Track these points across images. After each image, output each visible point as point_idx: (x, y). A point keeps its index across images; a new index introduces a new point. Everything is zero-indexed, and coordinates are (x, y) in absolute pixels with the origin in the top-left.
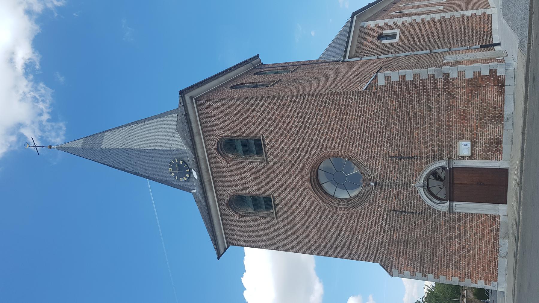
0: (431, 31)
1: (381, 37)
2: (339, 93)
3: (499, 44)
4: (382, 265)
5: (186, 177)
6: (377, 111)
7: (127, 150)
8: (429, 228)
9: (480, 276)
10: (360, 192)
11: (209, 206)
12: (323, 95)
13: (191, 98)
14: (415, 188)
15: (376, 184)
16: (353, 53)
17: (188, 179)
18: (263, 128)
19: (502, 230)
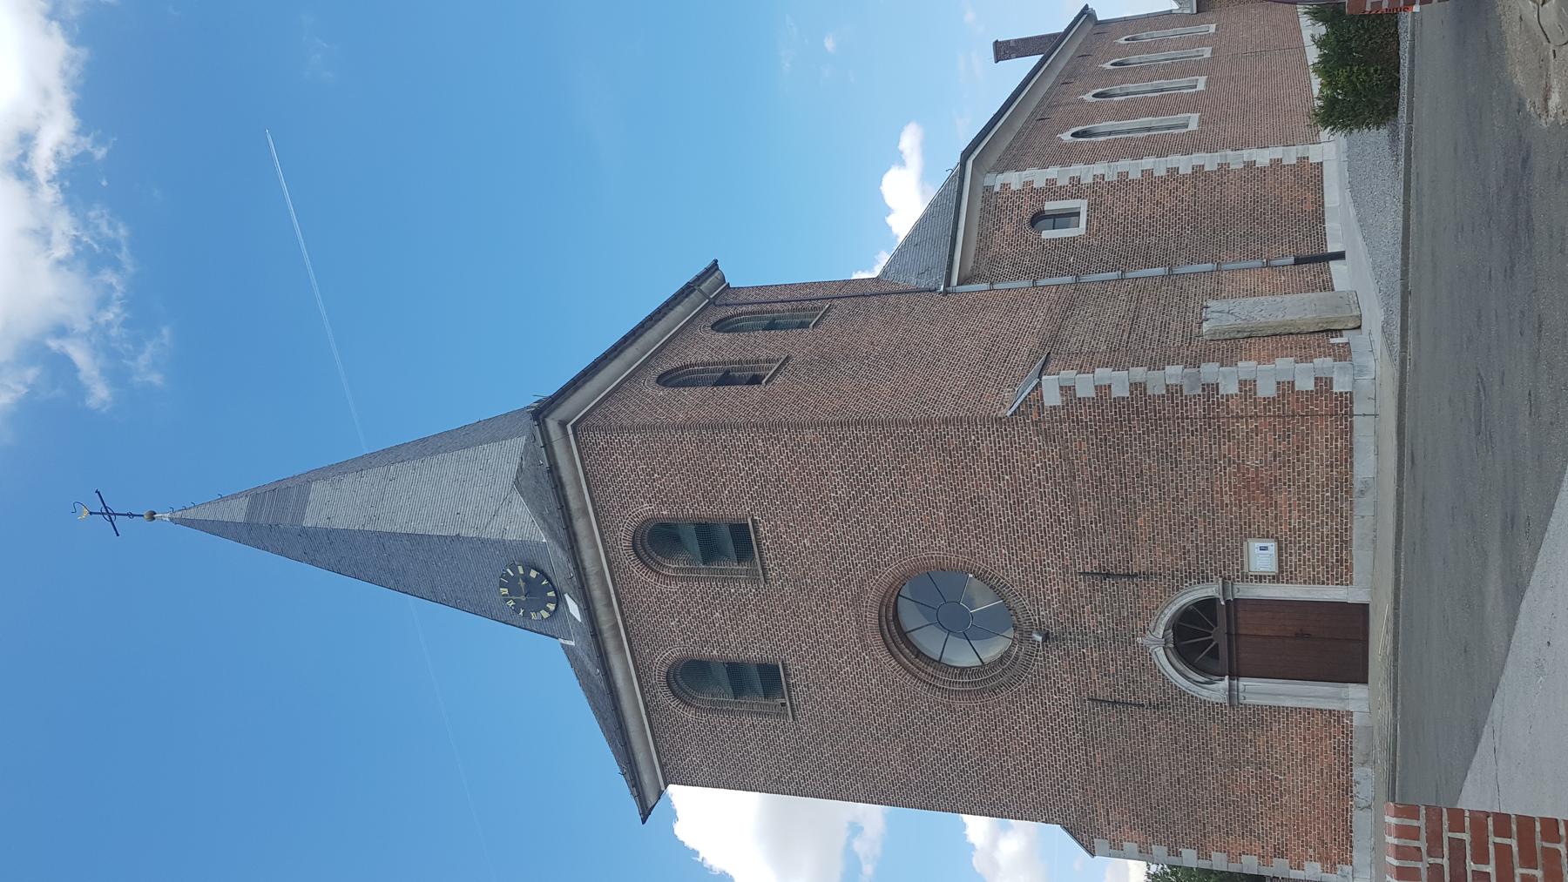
1: (1038, 218)
2: (946, 422)
3: (1340, 256)
4: (1067, 829)
5: (547, 610)
6: (1045, 466)
7: (380, 535)
8: (1182, 741)
9: (1311, 851)
10: (1007, 654)
12: (905, 423)
14: (1145, 648)
15: (1046, 637)
16: (970, 264)
17: (553, 614)
18: (753, 498)
19: (1359, 746)
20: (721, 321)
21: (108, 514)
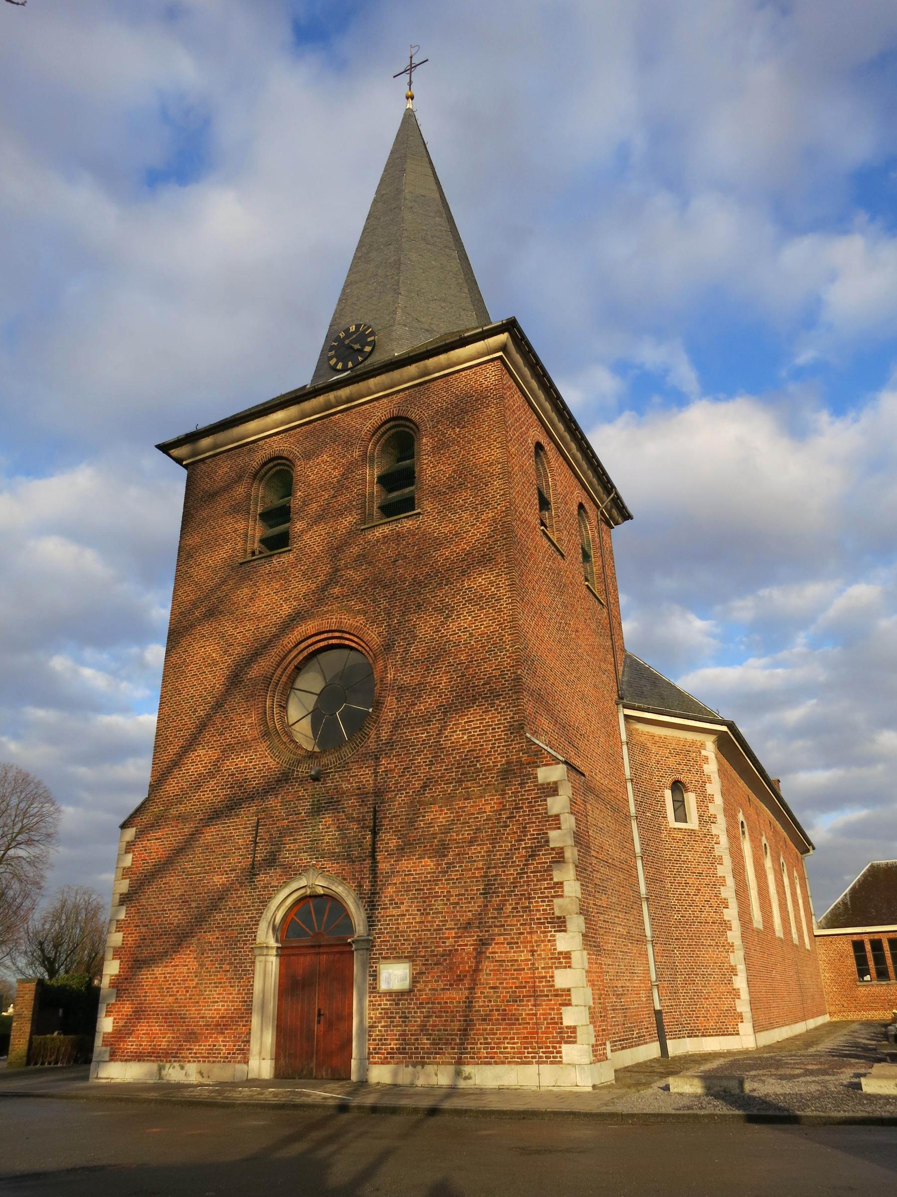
0: (697, 898)
1: (678, 787)
5: (336, 364)
11: (266, 415)
13: (504, 348)
20: (585, 511)
21: (411, 68)
